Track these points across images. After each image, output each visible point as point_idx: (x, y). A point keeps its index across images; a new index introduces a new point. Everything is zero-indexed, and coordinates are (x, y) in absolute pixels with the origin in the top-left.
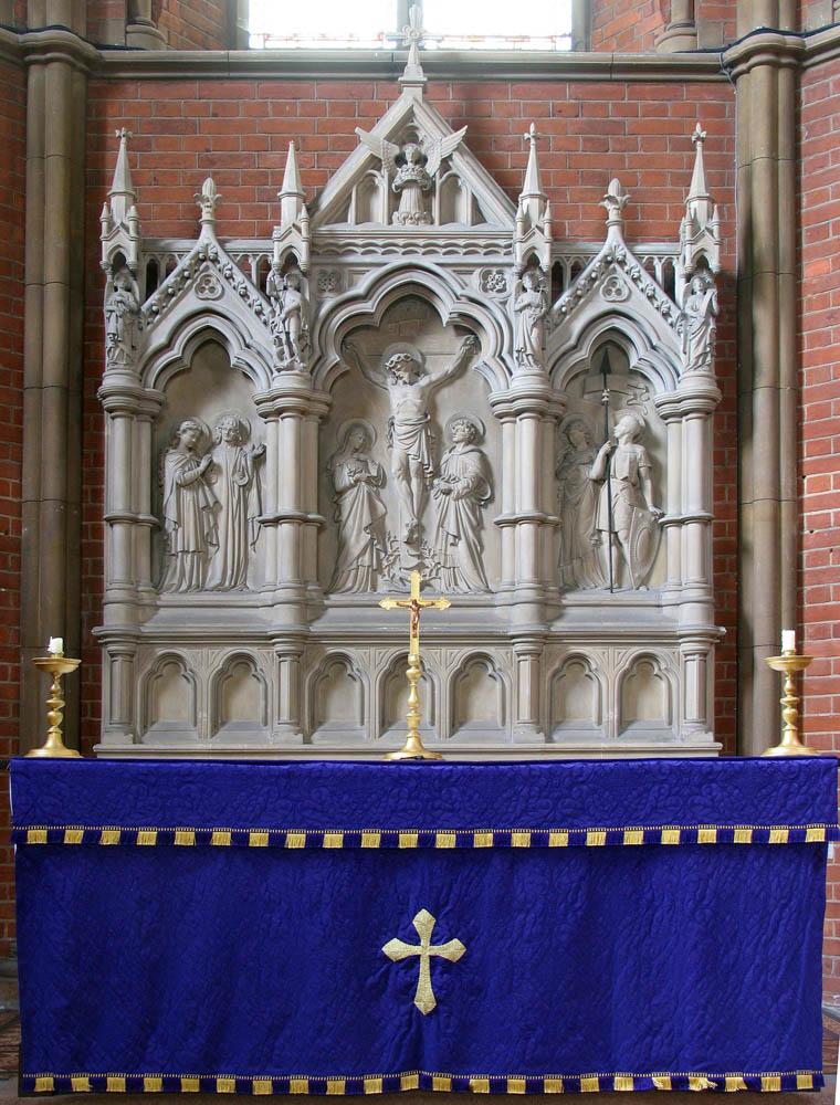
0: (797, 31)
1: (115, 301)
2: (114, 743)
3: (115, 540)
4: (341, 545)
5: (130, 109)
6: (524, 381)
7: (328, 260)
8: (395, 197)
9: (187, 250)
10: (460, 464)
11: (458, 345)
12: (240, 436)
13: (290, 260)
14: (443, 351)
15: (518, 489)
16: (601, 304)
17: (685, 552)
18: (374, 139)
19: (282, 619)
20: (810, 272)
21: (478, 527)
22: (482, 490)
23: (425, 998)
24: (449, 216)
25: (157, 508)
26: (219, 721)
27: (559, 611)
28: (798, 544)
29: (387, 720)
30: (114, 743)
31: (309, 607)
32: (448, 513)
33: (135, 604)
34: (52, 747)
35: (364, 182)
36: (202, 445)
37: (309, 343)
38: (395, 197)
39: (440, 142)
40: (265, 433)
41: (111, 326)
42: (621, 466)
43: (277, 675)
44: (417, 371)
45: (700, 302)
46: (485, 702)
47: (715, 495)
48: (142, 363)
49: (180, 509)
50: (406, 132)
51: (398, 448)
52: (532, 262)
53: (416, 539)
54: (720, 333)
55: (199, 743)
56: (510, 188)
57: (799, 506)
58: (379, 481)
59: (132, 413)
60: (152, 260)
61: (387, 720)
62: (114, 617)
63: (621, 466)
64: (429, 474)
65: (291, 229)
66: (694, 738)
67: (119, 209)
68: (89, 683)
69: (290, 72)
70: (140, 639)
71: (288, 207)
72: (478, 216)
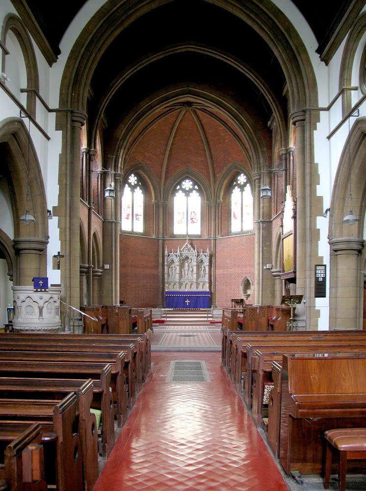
1: (166, 258)
5: (166, 242)
6: (195, 264)
10: (191, 269)
12: (175, 267)
15: (195, 271)
17: (207, 275)
18: (184, 246)
19: (178, 281)
20: (217, 255)
26: (173, 288)
29: (185, 288)
31: (180, 280)
32: (190, 273)
36: (172, 268)
39: (189, 246)
40: (177, 267)
43: (177, 285)
44: (187, 262)
46: (192, 286)
47: (323, 199)
50: (187, 245)
51: (186, 268)
55: (172, 290)
56: (194, 249)
58: (185, 270)
59: (167, 266)
61: (185, 288)
65: (178, 253)
66: (208, 290)
68: (239, 301)
69: (179, 236)
71: (178, 251)
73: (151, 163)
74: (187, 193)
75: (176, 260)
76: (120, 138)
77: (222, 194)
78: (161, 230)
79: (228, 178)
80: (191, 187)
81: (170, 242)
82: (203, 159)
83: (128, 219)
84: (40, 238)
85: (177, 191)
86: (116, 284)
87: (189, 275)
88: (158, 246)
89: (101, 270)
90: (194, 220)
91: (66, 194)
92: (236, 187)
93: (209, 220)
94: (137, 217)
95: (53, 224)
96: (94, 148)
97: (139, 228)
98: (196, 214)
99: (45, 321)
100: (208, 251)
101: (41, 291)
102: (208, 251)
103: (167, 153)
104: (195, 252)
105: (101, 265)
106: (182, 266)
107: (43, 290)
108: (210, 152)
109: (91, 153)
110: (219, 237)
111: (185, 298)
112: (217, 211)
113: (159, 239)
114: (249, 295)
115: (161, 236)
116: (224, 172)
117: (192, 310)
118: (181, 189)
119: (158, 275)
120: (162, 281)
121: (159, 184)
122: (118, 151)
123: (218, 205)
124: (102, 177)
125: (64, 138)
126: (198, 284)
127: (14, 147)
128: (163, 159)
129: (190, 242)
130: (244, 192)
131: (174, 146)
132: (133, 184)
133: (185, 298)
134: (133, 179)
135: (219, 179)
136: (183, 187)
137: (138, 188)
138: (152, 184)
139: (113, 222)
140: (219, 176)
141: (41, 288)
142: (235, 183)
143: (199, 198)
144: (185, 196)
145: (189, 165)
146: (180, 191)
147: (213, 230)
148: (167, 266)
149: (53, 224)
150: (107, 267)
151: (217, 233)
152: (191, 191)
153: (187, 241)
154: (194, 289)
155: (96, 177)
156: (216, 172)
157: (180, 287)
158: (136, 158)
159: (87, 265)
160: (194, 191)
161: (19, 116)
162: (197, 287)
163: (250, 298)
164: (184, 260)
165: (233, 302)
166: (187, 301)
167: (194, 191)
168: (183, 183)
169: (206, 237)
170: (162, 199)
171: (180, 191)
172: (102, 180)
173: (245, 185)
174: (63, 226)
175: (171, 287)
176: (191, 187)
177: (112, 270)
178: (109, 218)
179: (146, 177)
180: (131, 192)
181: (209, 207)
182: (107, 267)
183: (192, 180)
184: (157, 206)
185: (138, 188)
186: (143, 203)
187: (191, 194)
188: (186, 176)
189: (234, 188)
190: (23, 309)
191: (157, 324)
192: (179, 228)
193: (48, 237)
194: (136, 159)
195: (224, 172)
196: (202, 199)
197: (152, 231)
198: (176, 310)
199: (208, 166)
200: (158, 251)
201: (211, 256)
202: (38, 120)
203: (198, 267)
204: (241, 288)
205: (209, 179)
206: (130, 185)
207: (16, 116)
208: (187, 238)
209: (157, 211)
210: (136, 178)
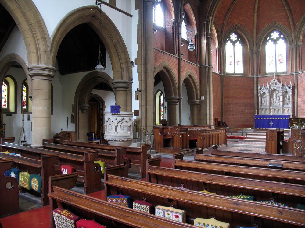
0: (297, 72)
1: (259, 91)
2: (259, 114)
3: (259, 103)
4: (271, 103)
5: (259, 79)
6: (281, 94)
7: (270, 88)
8: (274, 84)
9: (263, 87)
10: (278, 98)
11: (278, 91)
12: (266, 97)
13: (268, 88)
14: (277, 92)
15: (281, 100)
16: (286, 89)
17: (291, 103)
18: (272, 81)
19: (268, 107)
20: (298, 86)
21: (279, 102)
22: (279, 99)
23: (271, 125)
24: (277, 85)
25: (261, 101)
26: (265, 113)
27: (284, 106)
28: (298, 102)
30: (259, 114)
32: (277, 101)
33: (260, 107)
34: (256, 115)
35: (272, 83)
36: (264, 98)
37: (269, 92)
38: (274, 84)
39: (276, 81)
41: (259, 92)
42: (287, 98)
43: (268, 110)
44: (275, 93)
45: (291, 89)
46: (279, 112)
48: (260, 94)
49: (263, 101)
50: (274, 80)
51: (275, 97)
52: (281, 87)
53: (276, 102)
54: (73, 213)
56: (280, 83)
57: (298, 100)
58: (274, 99)
60: (194, 225)
62: (259, 107)
63: (287, 98)
64: (276, 99)
65: (268, 87)
67: (259, 86)
69: (270, 74)
70: (261, 109)
72: (278, 85)
74: (275, 41)
75: (267, 92)
76: (209, 9)
78: (255, 71)
80: (278, 36)
81: (262, 78)
82: (284, 14)
83: (231, 64)
84: (125, 79)
86: (210, 110)
87: (277, 102)
89: (198, 101)
91: (141, 50)
93: (292, 60)
94: (238, 63)
95: (135, 70)
96: (181, 18)
97: (240, 70)
98: (282, 57)
99: (118, 135)
100: (291, 84)
101: (115, 115)
102: (291, 84)
103: (256, 14)
105: (199, 97)
106: (271, 96)
107: (116, 114)
108: (289, 7)
109: (179, 22)
110: (299, 72)
111: (269, 121)
112: (298, 52)
113: (254, 78)
118: (270, 39)
119: (254, 104)
120: (256, 106)
122: (208, 18)
123: (298, 47)
124: (198, 37)
125: (140, 13)
127: (96, 24)
128: (253, 20)
129: (277, 78)
131: (260, 8)
132: (234, 40)
133: (269, 121)
134: (233, 37)
135: (298, 26)
136: (272, 37)
137: (238, 42)
138: (247, 38)
140: (298, 24)
141: (115, 112)
143: (285, 44)
144: (274, 43)
145: (274, 20)
146: (270, 41)
147: (294, 67)
148: (260, 96)
149: (135, 70)
150: (203, 98)
151: (298, 69)
152: (278, 39)
153: (275, 77)
154: (280, 113)
155: (194, 38)
158: (233, 21)
159: (178, 97)
160: (281, 39)
161: (95, 5)
162: (283, 112)
164: (272, 92)
166: (271, 123)
167: (281, 39)
168: (272, 34)
170: (255, 48)
171: (270, 41)
172: (198, 39)
174: (140, 71)
175: (263, 112)
176: (278, 36)
177: (206, 100)
178: (204, 65)
179: (242, 34)
180: (233, 46)
181: (292, 50)
182: (203, 98)
183: (278, 31)
187: (278, 42)
190: (108, 125)
191: (238, 140)
192: (270, 68)
193: (132, 80)
194: (233, 22)
196: (286, 45)
197: (249, 71)
198: (261, 129)
201: (293, 88)
202: (117, 6)
203: (284, 96)
206: (231, 41)
207: (94, 5)
208: (275, 75)
210: (236, 36)
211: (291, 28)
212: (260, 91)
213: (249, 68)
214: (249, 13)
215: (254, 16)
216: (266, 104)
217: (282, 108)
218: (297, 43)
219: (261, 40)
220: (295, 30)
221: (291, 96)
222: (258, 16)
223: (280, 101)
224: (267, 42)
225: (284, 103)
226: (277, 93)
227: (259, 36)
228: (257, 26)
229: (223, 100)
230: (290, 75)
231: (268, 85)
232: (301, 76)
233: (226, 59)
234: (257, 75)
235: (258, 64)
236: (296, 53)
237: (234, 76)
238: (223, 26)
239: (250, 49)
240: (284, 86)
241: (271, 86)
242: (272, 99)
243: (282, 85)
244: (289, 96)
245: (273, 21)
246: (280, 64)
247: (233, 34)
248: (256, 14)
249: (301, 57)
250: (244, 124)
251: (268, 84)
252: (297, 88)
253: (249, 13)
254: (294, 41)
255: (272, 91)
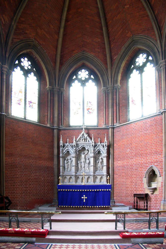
0: (113, 126)
1: (61, 149)
3: (61, 168)
4: (78, 168)
6: (92, 155)
7: (77, 145)
8: (82, 140)
9: (66, 144)
10: (88, 161)
11: (87, 152)
12: (71, 159)
14: (86, 152)
15: (92, 163)
17: (105, 168)
18: (81, 135)
19: (74, 174)
20: (115, 145)
21: (89, 166)
22: (89, 163)
23: (84, 201)
24: (86, 141)
25: (64, 165)
28: (114, 167)
29: (82, 182)
31: (76, 173)
32: (87, 165)
33: (63, 173)
35: (80, 139)
36: (68, 160)
38: (82, 140)
39: (86, 135)
41: (61, 151)
42: (100, 161)
43: (74, 178)
44: (84, 154)
45: (106, 148)
46: (90, 180)
48: (63, 154)
49: (66, 165)
50: (83, 135)
51: (83, 160)
52: (93, 145)
56: (91, 139)
57: (114, 164)
58: (81, 163)
59: (62, 158)
61: (82, 182)
63: (100, 161)
65: (74, 143)
67: (61, 142)
68: (144, 196)
72: (89, 141)
73: (44, 43)
74: (83, 82)
77: (119, 78)
78: (56, 119)
79: (127, 58)
81: (66, 132)
82: (99, 40)
85: (73, 81)
88: (53, 136)
90: (90, 110)
92: (135, 71)
93: (107, 107)
94: (31, 104)
100: (106, 140)
102: (106, 140)
103: (62, 30)
104: (92, 142)
106: (78, 158)
111: (81, 194)
112: (115, 97)
114: (155, 189)
115: (56, 126)
116: (121, 53)
117: (89, 209)
119: (53, 168)
121: (55, 69)
126: (95, 177)
130: (143, 74)
131: (69, 23)
133: (81, 194)
134: (26, 63)
135: (116, 62)
137: (32, 74)
139: (149, 228)
140: (116, 58)
142: (133, 66)
148: (63, 157)
151: (115, 121)
152: (86, 80)
153: (84, 130)
156: (113, 54)
157: (76, 181)
158: (27, 32)
160: (90, 81)
162: (94, 181)
163: (156, 193)
164: (81, 151)
165: (136, 198)
166: (84, 197)
168: (80, 73)
169: (104, 126)
171: (76, 81)
173: (145, 65)
176: (87, 77)
181: (106, 94)
184: (52, 92)
185: (32, 74)
186: (37, 91)
187: (87, 84)
188: (83, 53)
189: (131, 72)
191: (34, 239)
194: (27, 33)
195: (121, 53)
197: (46, 119)
199: (104, 48)
200: (53, 142)
201: (109, 147)
203: (96, 158)
204: (145, 180)
205: (106, 64)
209: (52, 98)
211: (107, 64)
212: (62, 150)
213: (46, 114)
214: (52, 27)
215: (58, 34)
216: (71, 170)
217: (94, 175)
218: (114, 85)
219: (66, 76)
220: (112, 67)
221: (105, 158)
222: (64, 35)
223: (90, 165)
224: (73, 82)
225: (96, 169)
226: (86, 153)
227: (63, 68)
228: (61, 53)
229: (4, 159)
230: (104, 129)
231: (74, 141)
232: (119, 130)
233: (13, 93)
234: (58, 125)
235: (60, 110)
236: (112, 99)
237: (25, 123)
238: (9, 29)
239: (50, 85)
240: (96, 144)
241: (79, 143)
242: (79, 162)
243: (94, 142)
244: (102, 159)
245: (84, 50)
246: (89, 114)
247: (26, 59)
248: (62, 30)
249: (119, 105)
250: (38, 199)
251: (74, 139)
252: (114, 150)
253: (52, 27)
254: (110, 81)
255: (79, 150)
